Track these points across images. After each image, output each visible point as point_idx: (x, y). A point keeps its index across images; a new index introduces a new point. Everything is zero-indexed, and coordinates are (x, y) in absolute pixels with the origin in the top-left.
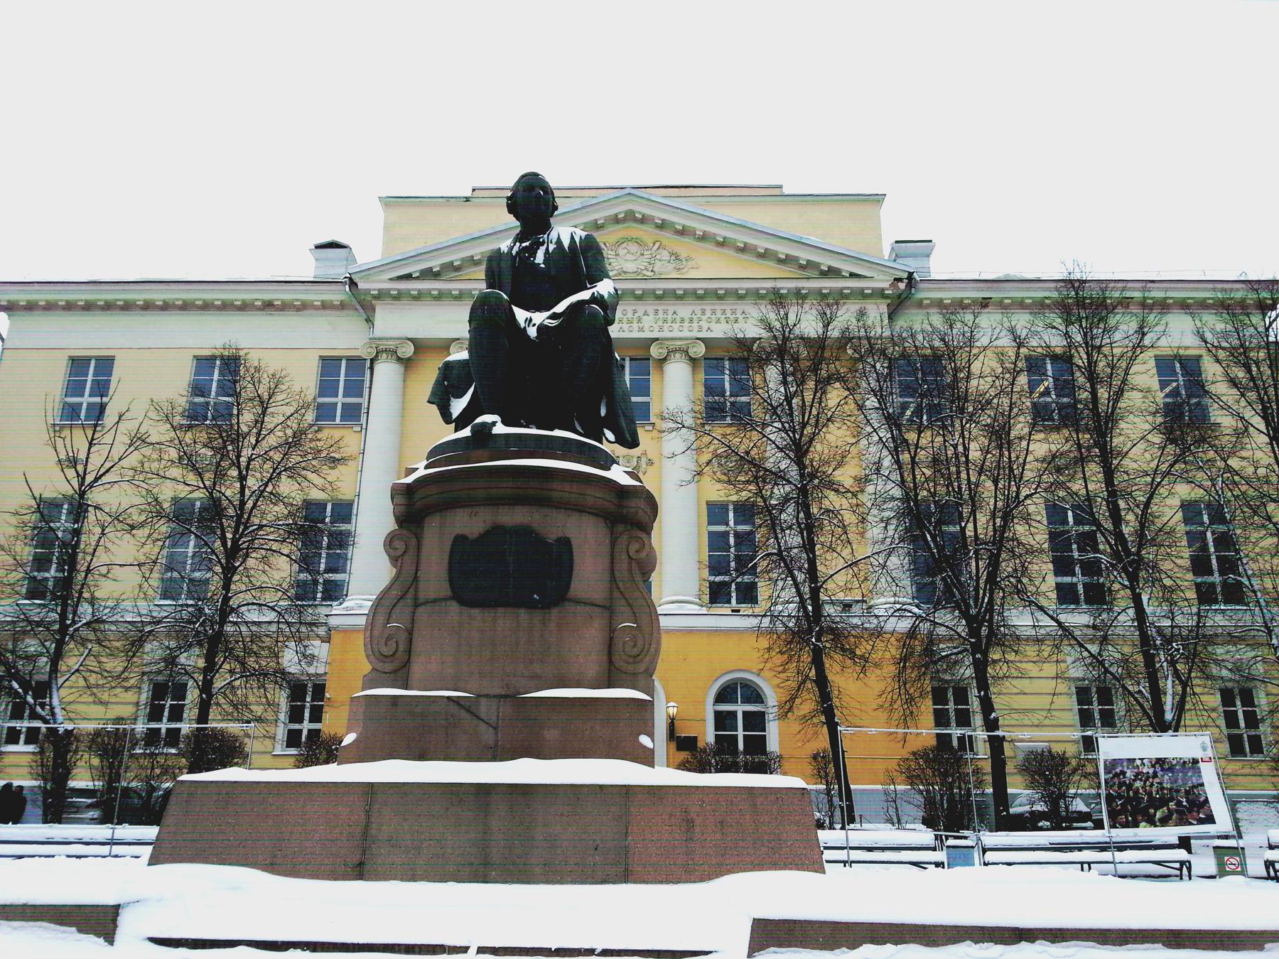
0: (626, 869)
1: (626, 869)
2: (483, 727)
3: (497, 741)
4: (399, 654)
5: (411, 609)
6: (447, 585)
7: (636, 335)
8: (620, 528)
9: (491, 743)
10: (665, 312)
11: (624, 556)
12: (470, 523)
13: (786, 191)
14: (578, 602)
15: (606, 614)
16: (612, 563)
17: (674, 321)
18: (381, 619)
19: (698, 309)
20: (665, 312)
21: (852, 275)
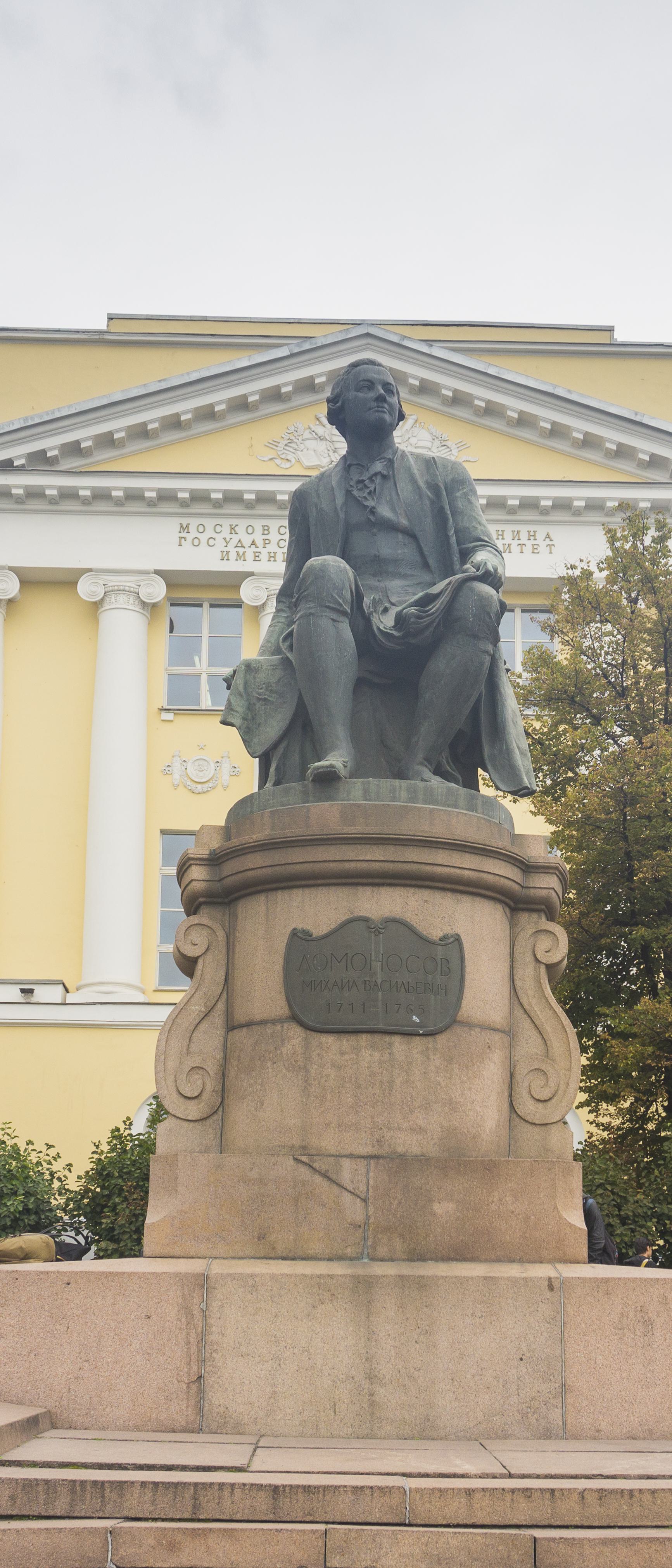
0: (563, 1385)
1: (563, 1385)
2: (347, 1198)
4: (205, 1096)
5: (220, 1032)
6: (283, 1002)
8: (524, 917)
9: (360, 1217)
11: (529, 958)
12: (320, 912)
13: (620, 336)
15: (506, 1039)
16: (512, 968)
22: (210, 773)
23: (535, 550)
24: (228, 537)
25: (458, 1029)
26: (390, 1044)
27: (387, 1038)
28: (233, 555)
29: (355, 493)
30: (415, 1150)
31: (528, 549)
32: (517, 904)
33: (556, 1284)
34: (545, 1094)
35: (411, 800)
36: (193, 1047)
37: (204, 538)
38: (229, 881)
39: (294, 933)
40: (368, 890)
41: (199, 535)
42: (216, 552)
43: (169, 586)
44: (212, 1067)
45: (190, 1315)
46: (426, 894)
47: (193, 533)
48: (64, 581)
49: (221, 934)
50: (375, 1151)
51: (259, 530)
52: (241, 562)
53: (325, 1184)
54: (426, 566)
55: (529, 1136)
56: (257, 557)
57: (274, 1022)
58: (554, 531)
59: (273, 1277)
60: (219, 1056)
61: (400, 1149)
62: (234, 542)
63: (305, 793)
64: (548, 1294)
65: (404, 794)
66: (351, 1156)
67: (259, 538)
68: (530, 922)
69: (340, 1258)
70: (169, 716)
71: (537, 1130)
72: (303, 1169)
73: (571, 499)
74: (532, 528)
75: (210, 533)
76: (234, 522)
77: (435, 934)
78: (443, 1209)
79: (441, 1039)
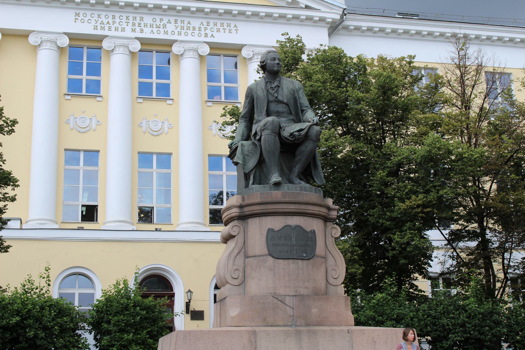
2: (288, 308)
3: (294, 313)
4: (240, 278)
5: (243, 258)
7: (162, 36)
9: (292, 314)
10: (182, 22)
14: (318, 256)
17: (188, 28)
18: (231, 262)
19: (205, 22)
20: (182, 22)
21: (307, 7)
22: (87, 123)
23: (230, 32)
24: (97, 19)
25: (315, 258)
26: (298, 262)
27: (297, 261)
28: (99, 28)
29: (270, 91)
30: (306, 294)
31: (227, 31)
32: (326, 219)
33: (350, 331)
34: (336, 276)
35: (300, 190)
36: (235, 263)
37: (86, 19)
38: (245, 213)
39: (269, 230)
40: (290, 217)
41: (84, 18)
42: (91, 26)
43: (70, 39)
44: (241, 269)
45: (251, 342)
46: (305, 218)
47: (81, 17)
48: (24, 35)
49: (242, 228)
50: (295, 294)
51: (111, 17)
52: (103, 31)
53: (282, 304)
54: (291, 113)
55: (331, 288)
56: (110, 29)
57: (263, 256)
58: (238, 24)
59: (273, 331)
60: (243, 265)
61: (302, 293)
62: (100, 22)
63: (270, 188)
64: (348, 334)
65: (299, 189)
66: (288, 296)
67: (111, 21)
68: (330, 225)
69: (287, 326)
70: (69, 97)
71: (334, 287)
72: (275, 299)
73: (245, 11)
74: (229, 22)
75: (89, 17)
76: (100, 13)
77: (308, 229)
78: (314, 311)
79: (311, 260)
